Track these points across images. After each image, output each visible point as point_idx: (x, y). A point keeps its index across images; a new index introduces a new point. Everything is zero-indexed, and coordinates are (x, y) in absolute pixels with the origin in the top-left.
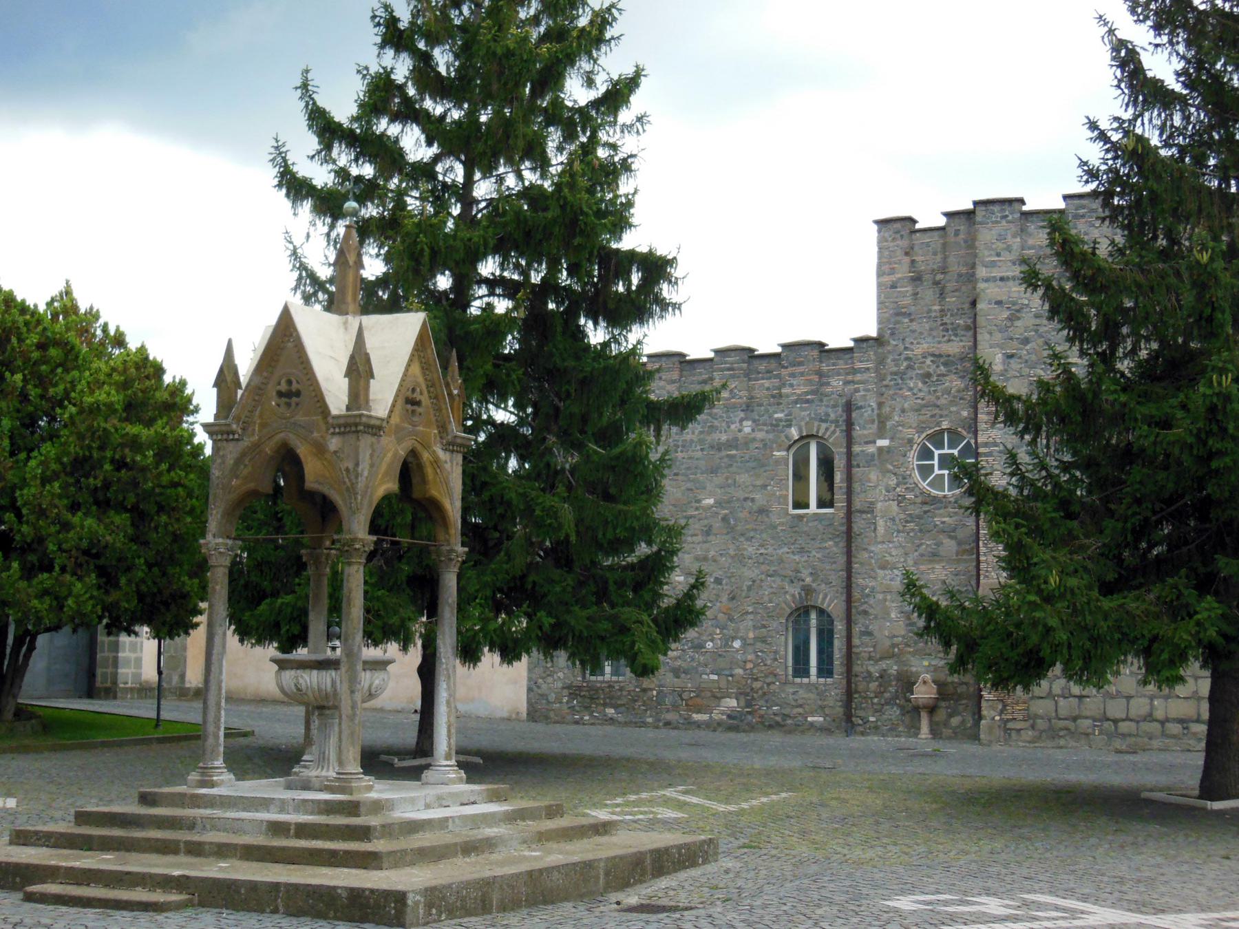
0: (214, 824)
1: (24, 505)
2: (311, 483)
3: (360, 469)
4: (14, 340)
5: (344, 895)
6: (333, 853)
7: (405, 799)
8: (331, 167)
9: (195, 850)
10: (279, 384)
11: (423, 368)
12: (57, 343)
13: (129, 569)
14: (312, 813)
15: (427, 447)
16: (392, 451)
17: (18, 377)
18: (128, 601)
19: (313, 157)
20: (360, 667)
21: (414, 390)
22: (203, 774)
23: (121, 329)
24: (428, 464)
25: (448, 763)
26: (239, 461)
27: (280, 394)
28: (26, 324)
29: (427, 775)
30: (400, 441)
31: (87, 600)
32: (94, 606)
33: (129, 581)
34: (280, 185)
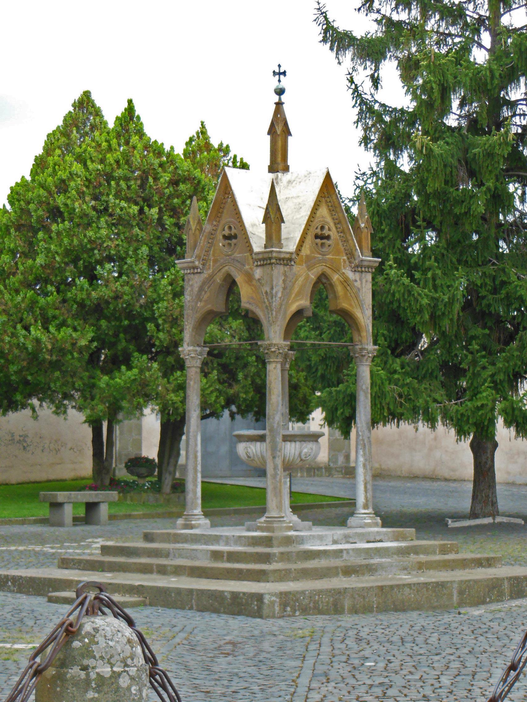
0: (180, 554)
1: (160, 316)
2: (245, 304)
3: (274, 292)
4: (151, 180)
5: (229, 596)
6: (240, 571)
7: (314, 536)
8: (375, 16)
9: (162, 570)
10: (224, 230)
11: (330, 210)
12: (186, 179)
13: (246, 365)
14: (244, 546)
15: (336, 270)
16: (304, 276)
17: (155, 211)
18: (246, 393)
19: (359, 9)
20: (279, 439)
21: (322, 228)
22: (186, 520)
23: (244, 161)
24: (337, 283)
25: (366, 511)
26: (201, 289)
27: (226, 237)
28: (161, 165)
29: (352, 521)
30: (309, 268)
31: (212, 392)
32: (217, 397)
33: (246, 377)
34: (324, 40)
